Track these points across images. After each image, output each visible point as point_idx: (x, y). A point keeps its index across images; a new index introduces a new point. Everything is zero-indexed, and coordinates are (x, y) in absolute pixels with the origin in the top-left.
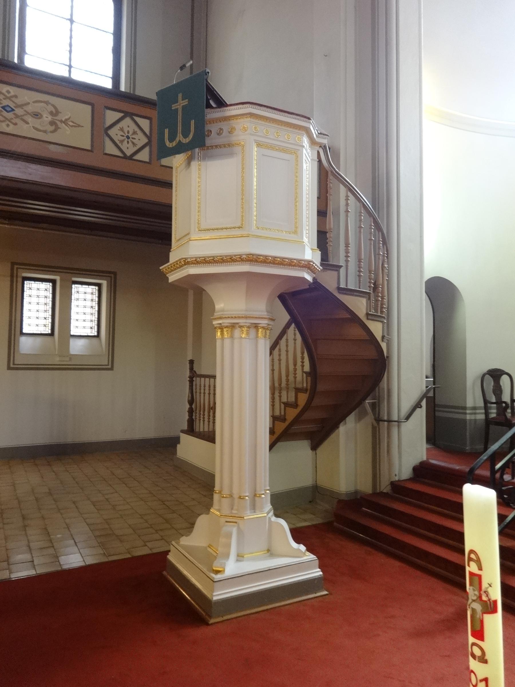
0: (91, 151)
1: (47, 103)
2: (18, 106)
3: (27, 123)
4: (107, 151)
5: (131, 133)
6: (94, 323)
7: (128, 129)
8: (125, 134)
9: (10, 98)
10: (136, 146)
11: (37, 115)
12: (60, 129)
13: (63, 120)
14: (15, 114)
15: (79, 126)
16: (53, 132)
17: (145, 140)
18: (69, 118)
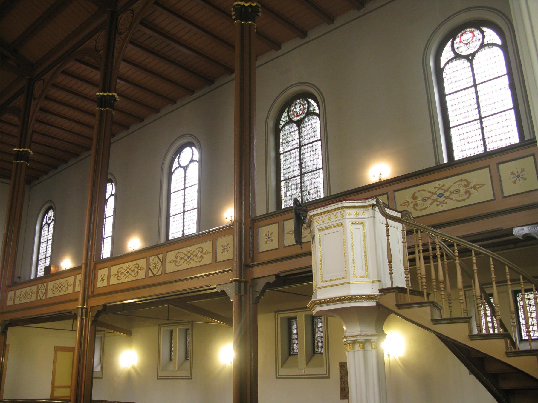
1: (462, 180)
5: (266, 237)
7: (269, 243)
11: (457, 191)
12: (472, 194)
14: (445, 197)
15: (483, 185)
16: (415, 193)
18: (408, 207)
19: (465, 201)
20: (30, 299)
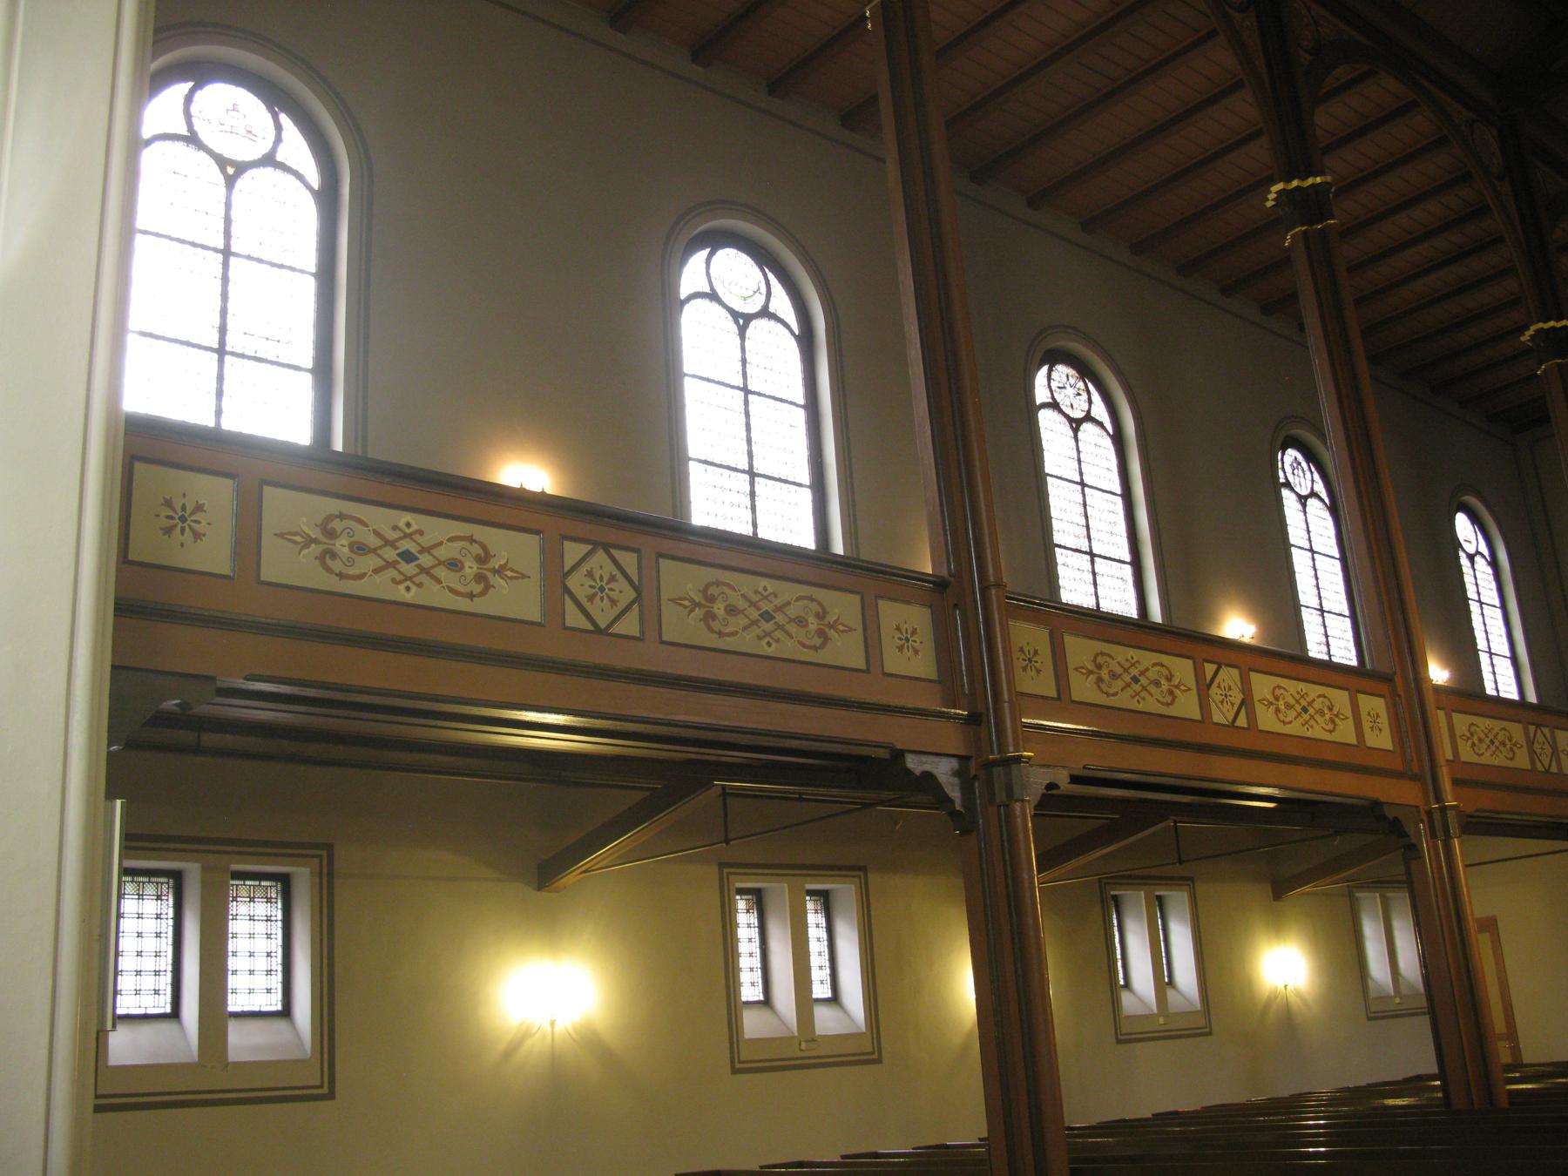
0: (867, 671)
2: (423, 550)
3: (439, 581)
4: (569, 623)
5: (606, 579)
6: (825, 985)
8: (178, 514)
9: (409, 536)
10: (616, 606)
13: (497, 567)
14: (419, 566)
15: (524, 576)
17: (632, 594)
18: (301, 550)
19: (472, 600)
20: (1480, 755)
